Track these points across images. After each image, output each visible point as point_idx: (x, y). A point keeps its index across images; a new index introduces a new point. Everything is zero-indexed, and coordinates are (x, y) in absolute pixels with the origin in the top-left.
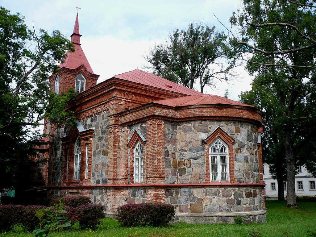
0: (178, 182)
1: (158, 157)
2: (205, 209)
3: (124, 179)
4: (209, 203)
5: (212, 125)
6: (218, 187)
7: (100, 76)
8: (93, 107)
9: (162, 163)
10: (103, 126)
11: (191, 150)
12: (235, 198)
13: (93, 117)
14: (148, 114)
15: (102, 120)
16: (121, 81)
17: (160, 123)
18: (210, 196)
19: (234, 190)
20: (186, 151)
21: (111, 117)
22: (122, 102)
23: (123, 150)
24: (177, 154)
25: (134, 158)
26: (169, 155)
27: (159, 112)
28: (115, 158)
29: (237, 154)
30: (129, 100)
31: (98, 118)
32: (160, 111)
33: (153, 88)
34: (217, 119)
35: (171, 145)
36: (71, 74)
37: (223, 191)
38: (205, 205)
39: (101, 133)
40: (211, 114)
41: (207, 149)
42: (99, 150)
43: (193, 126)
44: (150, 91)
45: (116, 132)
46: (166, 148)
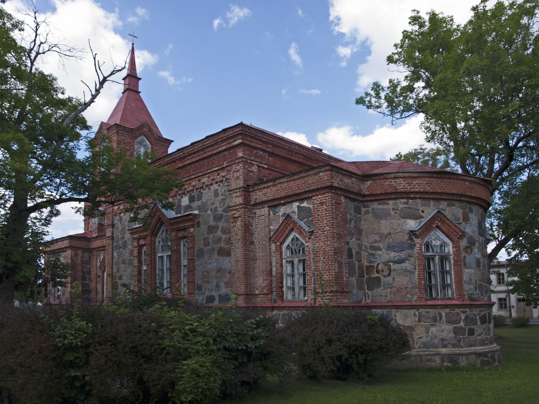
0: (366, 299)
1: (338, 259)
2: (417, 343)
3: (265, 294)
4: (424, 335)
5: (426, 208)
6: (440, 308)
7: (173, 141)
8: (193, 177)
9: (344, 268)
10: (217, 207)
11: (390, 248)
12: (465, 325)
13: (195, 193)
14: (319, 185)
15: (214, 198)
16: (252, 131)
17: (339, 200)
18: (426, 322)
19: (464, 312)
20: (380, 249)
21: (235, 191)
22: (253, 168)
23: (259, 248)
24: (364, 254)
25: (284, 261)
26: (352, 255)
27: (338, 181)
28: (246, 260)
29: (466, 255)
30: (265, 164)
31: (204, 195)
32: (340, 179)
33: (301, 148)
34: (435, 197)
35: (354, 239)
36: (129, 135)
37: (447, 314)
38: (417, 337)
39: (212, 219)
40: (426, 188)
41: (419, 246)
42: (210, 247)
43: (391, 208)
44: (296, 153)
45: (247, 217)
46: (348, 243)
